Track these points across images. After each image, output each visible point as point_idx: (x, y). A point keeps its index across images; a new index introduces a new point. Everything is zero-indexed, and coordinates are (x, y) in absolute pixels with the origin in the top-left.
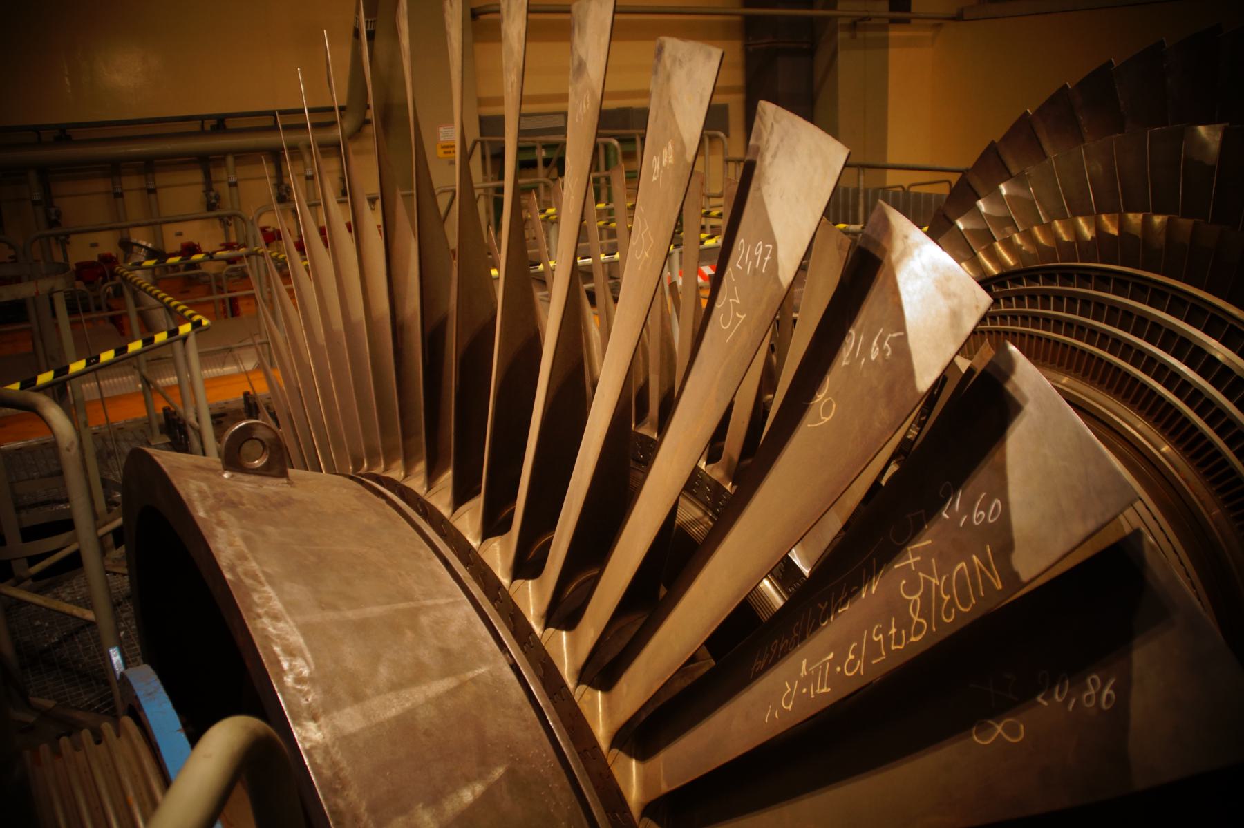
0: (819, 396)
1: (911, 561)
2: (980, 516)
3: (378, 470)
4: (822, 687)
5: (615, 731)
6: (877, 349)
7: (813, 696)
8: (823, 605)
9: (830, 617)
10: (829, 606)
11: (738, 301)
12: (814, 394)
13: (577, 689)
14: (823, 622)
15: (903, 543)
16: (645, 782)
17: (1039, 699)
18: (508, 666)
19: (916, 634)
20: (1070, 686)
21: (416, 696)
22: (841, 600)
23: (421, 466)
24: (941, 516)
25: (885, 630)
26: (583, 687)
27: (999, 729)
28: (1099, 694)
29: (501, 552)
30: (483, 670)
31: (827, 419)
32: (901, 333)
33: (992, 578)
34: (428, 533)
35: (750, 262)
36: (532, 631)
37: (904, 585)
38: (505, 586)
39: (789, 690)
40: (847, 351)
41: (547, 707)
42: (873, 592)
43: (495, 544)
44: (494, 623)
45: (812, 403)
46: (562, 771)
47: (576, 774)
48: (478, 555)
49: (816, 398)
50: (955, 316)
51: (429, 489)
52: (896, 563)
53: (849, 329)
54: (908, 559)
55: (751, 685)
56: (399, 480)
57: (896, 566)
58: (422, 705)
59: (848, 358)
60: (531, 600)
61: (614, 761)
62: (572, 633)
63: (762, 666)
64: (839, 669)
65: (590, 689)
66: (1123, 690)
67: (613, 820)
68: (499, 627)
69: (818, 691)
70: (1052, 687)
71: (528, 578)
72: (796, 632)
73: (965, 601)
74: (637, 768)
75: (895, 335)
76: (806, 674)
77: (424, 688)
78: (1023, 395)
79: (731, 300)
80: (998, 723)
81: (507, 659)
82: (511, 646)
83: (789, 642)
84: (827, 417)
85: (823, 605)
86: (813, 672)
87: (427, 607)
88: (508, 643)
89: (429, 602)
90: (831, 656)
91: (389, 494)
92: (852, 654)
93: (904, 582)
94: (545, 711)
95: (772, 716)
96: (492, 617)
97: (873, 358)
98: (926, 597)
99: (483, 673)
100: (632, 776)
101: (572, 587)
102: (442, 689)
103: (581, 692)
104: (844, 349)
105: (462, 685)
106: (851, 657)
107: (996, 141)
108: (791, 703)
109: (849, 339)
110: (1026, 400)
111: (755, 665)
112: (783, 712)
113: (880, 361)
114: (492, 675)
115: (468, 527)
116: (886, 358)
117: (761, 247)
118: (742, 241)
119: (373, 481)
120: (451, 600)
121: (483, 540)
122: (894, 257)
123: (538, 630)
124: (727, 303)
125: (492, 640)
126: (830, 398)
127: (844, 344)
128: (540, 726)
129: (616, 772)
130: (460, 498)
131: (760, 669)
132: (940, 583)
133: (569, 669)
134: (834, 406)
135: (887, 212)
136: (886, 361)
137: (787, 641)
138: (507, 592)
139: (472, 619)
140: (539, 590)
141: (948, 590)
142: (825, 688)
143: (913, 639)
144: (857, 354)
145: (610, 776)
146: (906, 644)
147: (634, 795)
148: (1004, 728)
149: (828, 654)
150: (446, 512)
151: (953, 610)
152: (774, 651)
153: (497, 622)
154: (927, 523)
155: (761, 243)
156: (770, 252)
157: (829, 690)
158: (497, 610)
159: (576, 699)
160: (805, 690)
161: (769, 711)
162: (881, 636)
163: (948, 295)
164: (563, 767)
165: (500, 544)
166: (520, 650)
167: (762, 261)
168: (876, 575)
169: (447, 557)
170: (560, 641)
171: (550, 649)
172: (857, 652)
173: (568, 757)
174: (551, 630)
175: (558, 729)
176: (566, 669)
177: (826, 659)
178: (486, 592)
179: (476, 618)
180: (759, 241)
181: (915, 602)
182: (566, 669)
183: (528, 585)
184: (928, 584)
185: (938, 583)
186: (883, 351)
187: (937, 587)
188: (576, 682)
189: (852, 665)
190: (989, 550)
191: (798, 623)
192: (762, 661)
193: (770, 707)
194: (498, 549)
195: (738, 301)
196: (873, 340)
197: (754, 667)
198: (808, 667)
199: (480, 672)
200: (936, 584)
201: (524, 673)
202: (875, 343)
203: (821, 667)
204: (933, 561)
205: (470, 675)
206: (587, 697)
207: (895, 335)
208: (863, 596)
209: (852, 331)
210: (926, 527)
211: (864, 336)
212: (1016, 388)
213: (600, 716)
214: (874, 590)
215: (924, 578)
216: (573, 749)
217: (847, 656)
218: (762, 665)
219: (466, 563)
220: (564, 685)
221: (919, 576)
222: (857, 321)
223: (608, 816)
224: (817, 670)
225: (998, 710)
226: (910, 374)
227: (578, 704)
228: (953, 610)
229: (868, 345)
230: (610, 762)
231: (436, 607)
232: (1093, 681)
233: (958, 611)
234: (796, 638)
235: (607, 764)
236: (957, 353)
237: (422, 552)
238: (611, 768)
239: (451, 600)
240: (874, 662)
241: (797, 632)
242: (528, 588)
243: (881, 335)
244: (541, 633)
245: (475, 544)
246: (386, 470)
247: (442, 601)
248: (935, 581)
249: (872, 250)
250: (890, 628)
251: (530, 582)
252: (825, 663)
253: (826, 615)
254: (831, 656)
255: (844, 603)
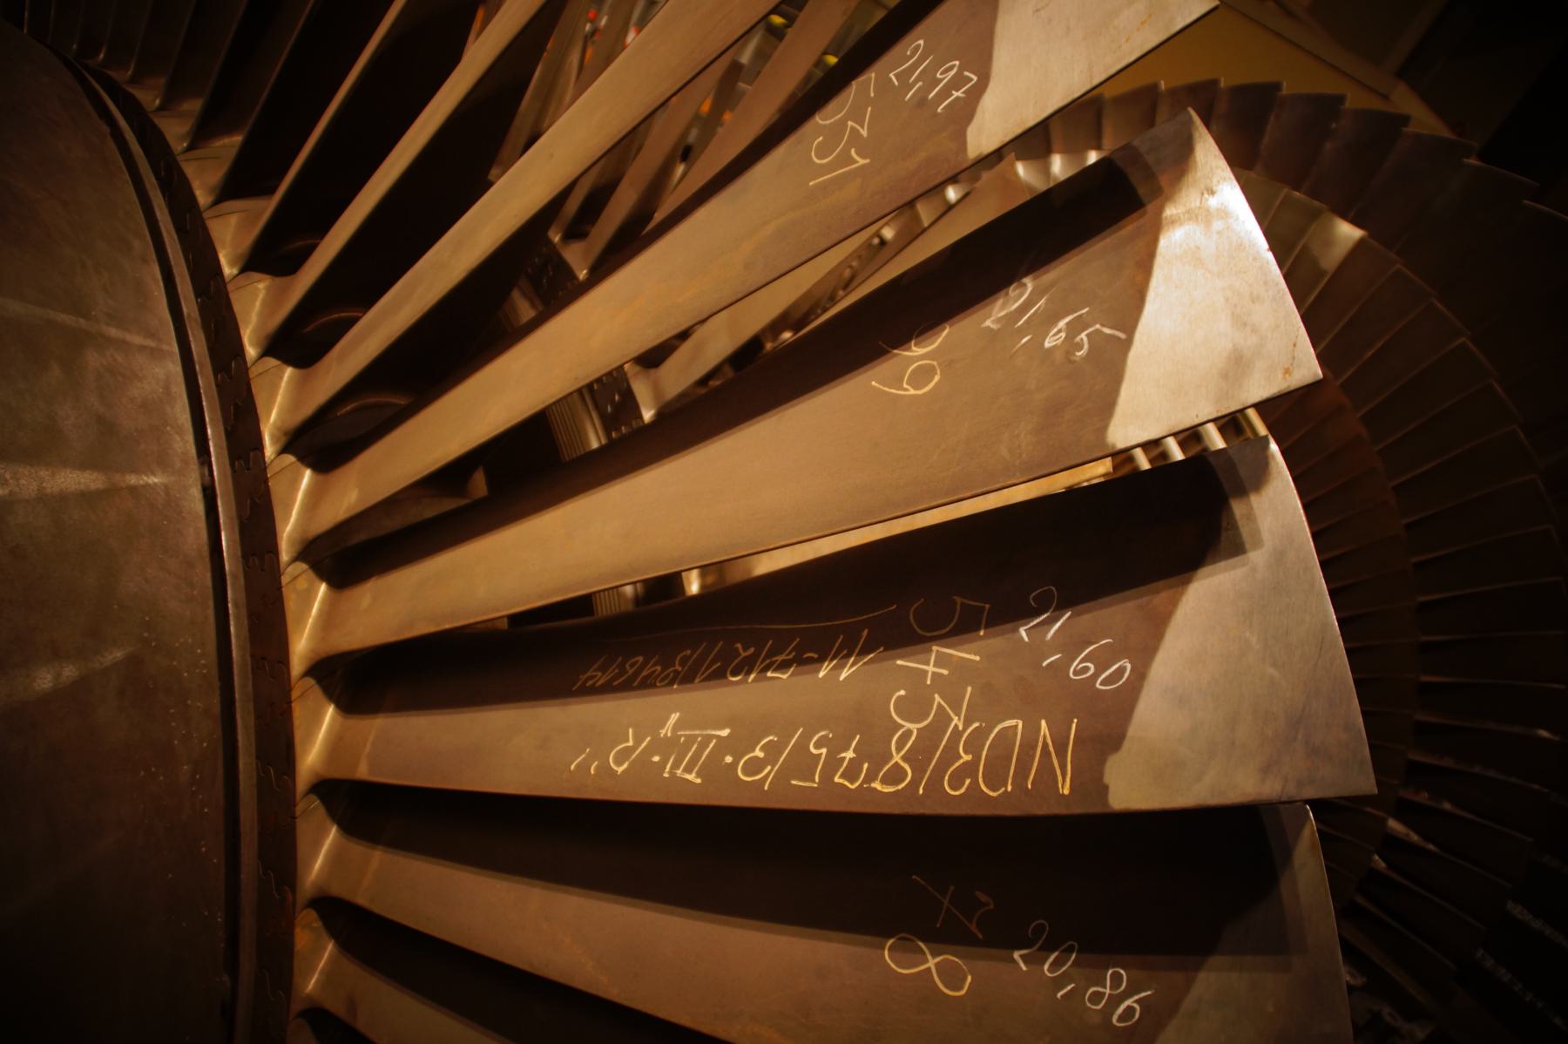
0: (914, 348)
1: (931, 669)
2: (1086, 669)
3: (122, 76)
4: (688, 770)
5: (323, 655)
6: (1063, 335)
7: (666, 775)
8: (745, 649)
9: (749, 673)
10: (755, 657)
11: (864, 133)
12: (908, 340)
13: (291, 567)
14: (734, 674)
15: (929, 634)
16: (336, 746)
17: (1016, 955)
18: (199, 487)
19: (884, 781)
20: (1075, 963)
21: (23, 482)
22: (780, 658)
23: (195, 106)
24: (1016, 630)
25: (836, 747)
26: (302, 566)
27: (932, 963)
28: (1116, 1001)
29: (265, 303)
30: (156, 480)
31: (912, 392)
32: (1122, 336)
33: (1060, 778)
34: (158, 214)
35: (920, 84)
36: (260, 446)
37: (900, 697)
38: (248, 359)
39: (631, 743)
40: (1002, 308)
41: (235, 577)
42: (842, 678)
43: (261, 286)
44: (205, 409)
45: (896, 351)
46: (217, 684)
47: (237, 696)
48: (226, 289)
49: (909, 349)
50: (1238, 365)
51: (191, 148)
52: (901, 657)
53: (1026, 275)
54: (927, 663)
55: (570, 700)
56: (176, 153)
57: (899, 662)
58: (27, 501)
59: (998, 320)
60: (279, 399)
61: (302, 695)
62: (321, 477)
63: (600, 683)
64: (729, 759)
65: (311, 574)
66: (1156, 1016)
67: (262, 775)
68: (211, 419)
69: (679, 772)
70: (1048, 948)
71: (288, 361)
72: (680, 665)
73: (994, 780)
74: (333, 720)
75: (1107, 331)
76: (669, 735)
77: (43, 473)
78: (1256, 533)
79: (850, 123)
80: (934, 955)
81: (202, 476)
82: (217, 458)
83: (662, 672)
84: (916, 388)
85: (745, 649)
86: (682, 739)
87: (109, 341)
88: (215, 450)
89: (113, 332)
90: (725, 733)
91: (122, 123)
92: (762, 749)
93: (902, 693)
94: (229, 582)
95: (584, 767)
96: (207, 400)
97: (1047, 344)
98: (929, 739)
99: (155, 484)
100: (320, 728)
101: (349, 408)
102: (74, 487)
103: (297, 572)
104: (1000, 302)
105: (110, 492)
106: (759, 753)
107: (1285, 91)
108: (625, 766)
109: (1017, 292)
110: (1258, 544)
111: (589, 674)
112: (605, 769)
113: (1059, 356)
114: (168, 494)
115: (229, 238)
116: (1073, 358)
117: (955, 70)
118: (921, 42)
119: (102, 88)
120: (151, 343)
121: (243, 271)
122: (1170, 211)
123: (269, 450)
124: (842, 124)
125: (190, 437)
126: (935, 363)
127: (1003, 292)
128: (211, 603)
129: (299, 711)
130: (235, 187)
131: (595, 683)
132: (964, 730)
133: (293, 530)
134: (937, 378)
135: (1196, 135)
136: (1071, 362)
137: (659, 668)
138: (247, 369)
139: (174, 389)
140: (299, 388)
141: (974, 745)
142: (694, 775)
143: (877, 785)
144: (1020, 324)
145: (287, 714)
146: (861, 785)
147: (312, 756)
148: (937, 965)
149: (722, 728)
150: (203, 198)
151: (968, 782)
152: (631, 672)
153: (211, 410)
154: (986, 627)
155: (957, 63)
156: (970, 84)
157: (699, 781)
158: (217, 385)
159: (285, 580)
160: (656, 759)
161: (583, 756)
162: (824, 751)
163: (1240, 321)
164: (221, 678)
165: (268, 289)
166: (228, 467)
167: (945, 92)
168: (858, 655)
169: (175, 271)
170: (296, 482)
171: (277, 487)
172: (773, 751)
173: (235, 666)
174: (290, 459)
175: (237, 618)
176: (289, 528)
177: (713, 733)
178: (211, 350)
179: (180, 389)
180: (956, 60)
181: (908, 733)
182: (289, 528)
183: (283, 373)
184: (942, 719)
185: (961, 728)
186: (1071, 344)
187: (957, 734)
188: (295, 555)
189: (754, 766)
190: (1074, 726)
191: (689, 652)
192: (604, 674)
193: (588, 750)
194: (261, 296)
195: (864, 133)
196: (1063, 317)
197: (586, 676)
198: (676, 727)
199: (150, 481)
200: (956, 726)
201: (220, 509)
202: (1062, 324)
203: (699, 739)
204: (969, 689)
205: (133, 480)
206: (302, 584)
207: (1107, 331)
208: (821, 674)
209: (1029, 283)
210: (982, 633)
211: (1047, 300)
212: (1251, 517)
213: (311, 620)
214: (844, 675)
215: (939, 704)
216: (249, 658)
217: (753, 750)
218: (602, 680)
219: (200, 291)
220: (274, 550)
221: (934, 699)
222: (1045, 273)
223: (257, 764)
224: (691, 740)
225: (944, 935)
226: (1106, 406)
227: (283, 589)
228: (968, 782)
229: (1050, 318)
230: (295, 694)
231: (123, 345)
232: (1117, 979)
233: (975, 784)
234: (676, 672)
235: (290, 696)
236: (1214, 420)
237: (137, 244)
238: (293, 705)
239: (151, 343)
240: (794, 782)
241: (683, 663)
242: (281, 378)
243: (1081, 316)
244: (272, 458)
245: (228, 270)
246: (133, 81)
247: (137, 340)
248: (957, 721)
249: (1135, 178)
250: (846, 749)
251: (289, 372)
252: (711, 737)
253: (745, 667)
254: (725, 733)
255: (783, 666)
